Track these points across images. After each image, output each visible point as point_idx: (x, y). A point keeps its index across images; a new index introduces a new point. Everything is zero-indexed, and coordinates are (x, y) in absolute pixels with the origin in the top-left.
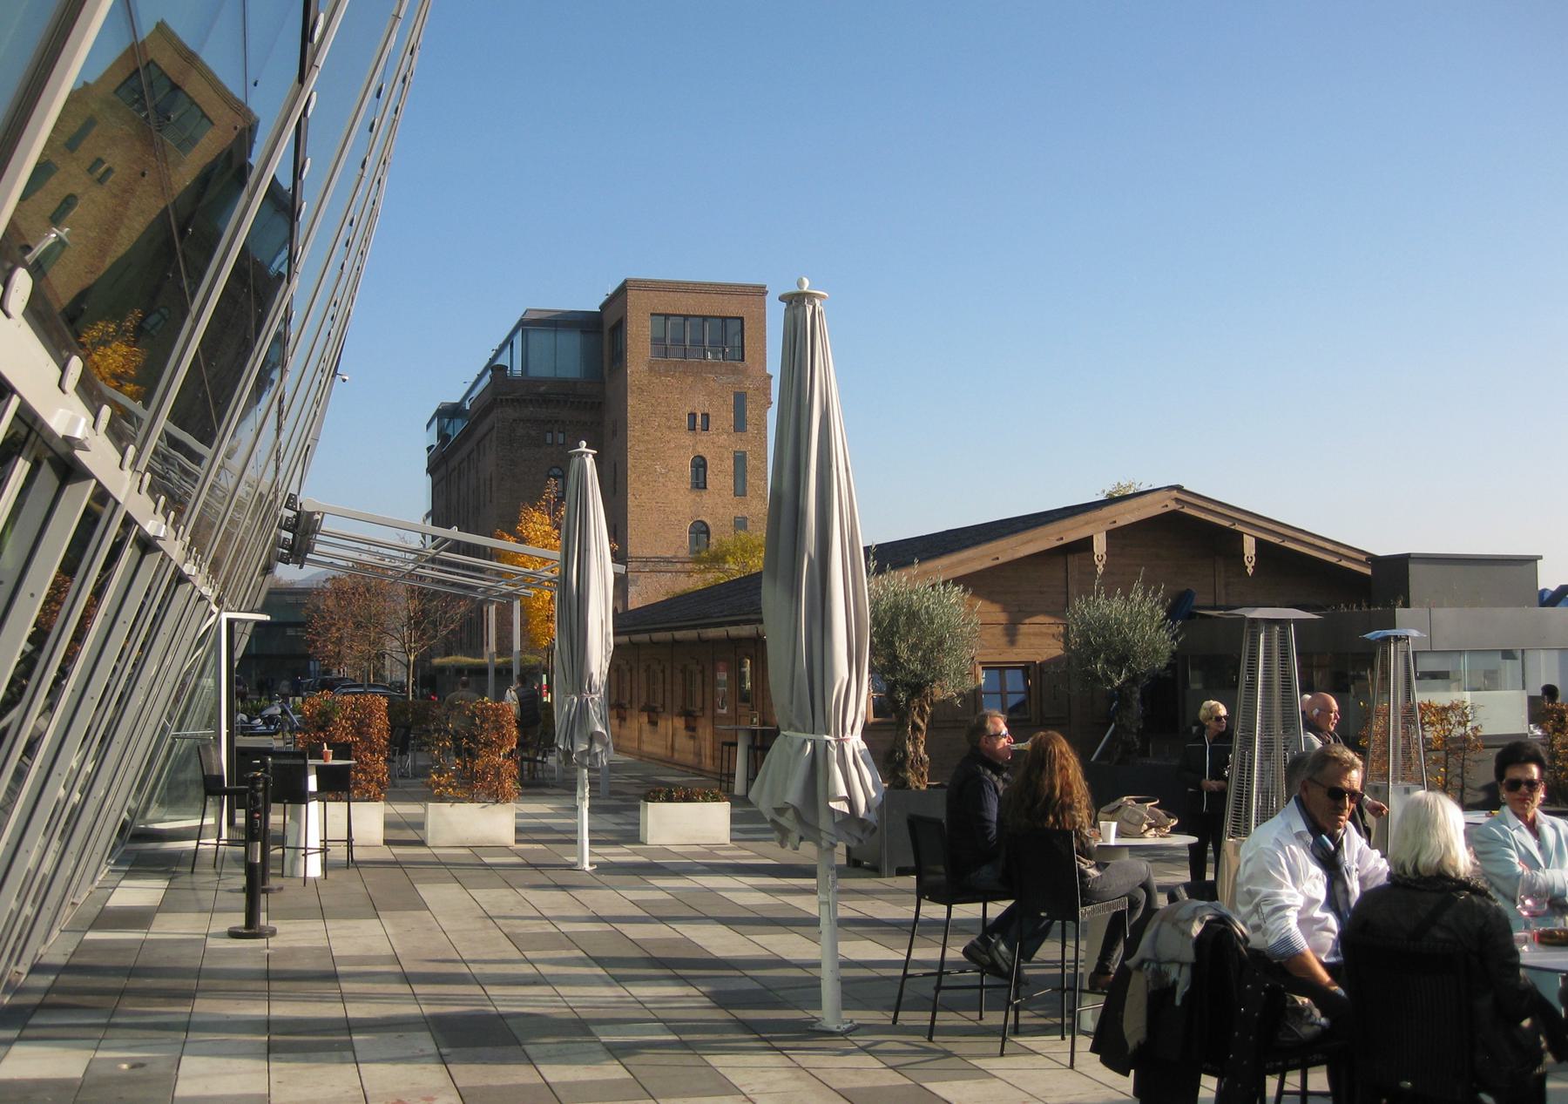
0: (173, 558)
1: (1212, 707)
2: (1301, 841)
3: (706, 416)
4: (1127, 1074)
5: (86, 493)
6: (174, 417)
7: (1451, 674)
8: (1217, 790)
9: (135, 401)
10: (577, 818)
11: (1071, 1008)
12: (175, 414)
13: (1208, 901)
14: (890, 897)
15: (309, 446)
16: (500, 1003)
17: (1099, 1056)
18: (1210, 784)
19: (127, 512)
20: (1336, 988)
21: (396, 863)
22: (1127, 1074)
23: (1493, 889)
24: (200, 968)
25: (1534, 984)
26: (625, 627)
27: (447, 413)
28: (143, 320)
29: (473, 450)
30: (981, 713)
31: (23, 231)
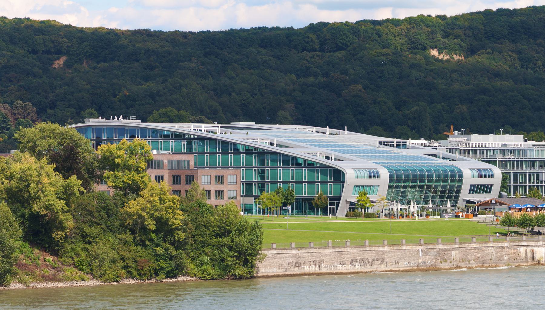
0: (223, 204)
1: (24, 179)
2: (440, 244)
3: (398, 261)
4: (327, 128)
7: (175, 173)
8: (37, 27)
9: (99, 118)
10: (449, 152)
11: (318, 190)
12: (255, 34)
13: (428, 138)
14: (270, 152)
15: (94, 148)
16: (489, 223)
17: (315, 24)
18: (203, 287)
19: (496, 166)
20: (456, 57)
21: (195, 170)
22: (327, 128)
23: (427, 144)
24: (255, 277)
25: (420, 140)
26: (405, 267)
27: (241, 28)
28: (408, 126)
29: (89, 252)
30: (458, 55)
31: (533, 236)
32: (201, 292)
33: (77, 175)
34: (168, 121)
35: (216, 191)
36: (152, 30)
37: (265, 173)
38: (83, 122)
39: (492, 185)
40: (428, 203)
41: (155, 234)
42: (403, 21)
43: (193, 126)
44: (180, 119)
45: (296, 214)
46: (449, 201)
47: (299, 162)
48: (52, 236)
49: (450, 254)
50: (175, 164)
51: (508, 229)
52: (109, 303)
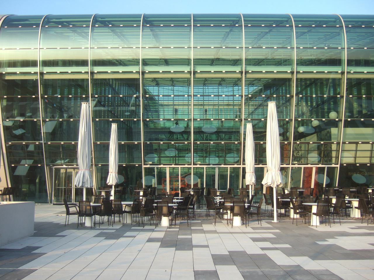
5: (40, 113)
6: (304, 168)
32: (287, 33)
33: (277, 223)
34: (241, 28)
35: (245, 167)
36: (231, 59)
37: (140, 41)
38: (55, 196)
39: (212, 255)
40: (232, 171)
41: (165, 221)
42: (366, 179)
43: (72, 202)
44: (42, 136)
45: (244, 164)
46: (272, 106)
47: (318, 217)
48: (194, 193)
49: (132, 221)
50: (117, 206)
51: (179, 160)
52: (258, 83)
